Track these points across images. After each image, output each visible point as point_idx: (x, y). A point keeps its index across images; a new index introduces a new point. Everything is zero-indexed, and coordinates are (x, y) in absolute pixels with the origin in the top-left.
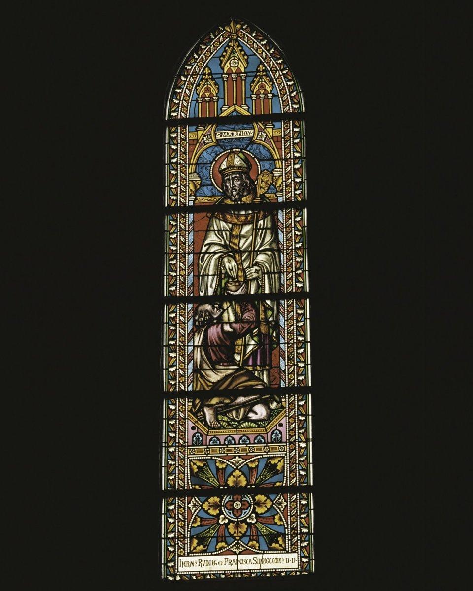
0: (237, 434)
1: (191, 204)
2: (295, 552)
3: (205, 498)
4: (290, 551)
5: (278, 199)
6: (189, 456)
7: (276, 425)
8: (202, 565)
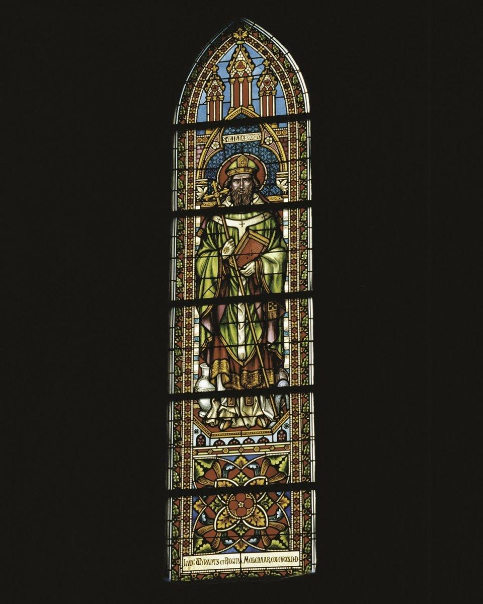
0: (241, 436)
1: (198, 208)
2: (297, 550)
6: (194, 457)
8: (204, 563)
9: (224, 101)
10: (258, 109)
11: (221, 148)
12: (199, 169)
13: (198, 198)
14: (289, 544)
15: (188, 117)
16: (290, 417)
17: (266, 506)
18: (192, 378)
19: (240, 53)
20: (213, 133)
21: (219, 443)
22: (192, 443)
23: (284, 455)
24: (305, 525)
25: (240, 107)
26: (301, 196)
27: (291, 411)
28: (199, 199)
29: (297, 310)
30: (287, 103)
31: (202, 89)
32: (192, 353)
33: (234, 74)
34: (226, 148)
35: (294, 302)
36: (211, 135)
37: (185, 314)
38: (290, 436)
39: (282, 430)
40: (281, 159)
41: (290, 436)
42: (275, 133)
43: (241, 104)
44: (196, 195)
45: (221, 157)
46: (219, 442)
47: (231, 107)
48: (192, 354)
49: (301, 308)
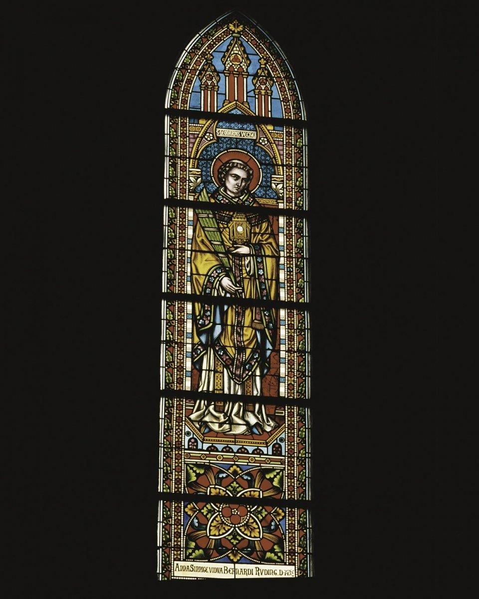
1: (191, 198)
3: (205, 504)
4: (287, 564)
5: (278, 206)
6: (186, 460)
7: (277, 439)
9: (218, 92)
10: (255, 110)
11: (215, 139)
12: (192, 158)
13: (192, 188)
14: (284, 557)
15: (178, 241)
16: (285, 431)
17: (259, 515)
18: (186, 280)
19: (236, 45)
20: (206, 123)
21: (212, 449)
22: (183, 444)
23: (278, 469)
24: (299, 345)
25: (235, 102)
26: (298, 327)
27: (287, 424)
28: (192, 190)
29: (294, 441)
30: (283, 107)
31: (196, 76)
32: (185, 348)
33: (229, 66)
34: (220, 142)
35: (291, 408)
36: (204, 125)
37: (175, 406)
38: (285, 449)
39: (277, 443)
40: (276, 162)
41: (285, 449)
42: (271, 135)
43: (236, 99)
44: (189, 185)
45: (216, 149)
46: (213, 448)
47: (226, 99)
48: (185, 350)
49: (297, 289)
